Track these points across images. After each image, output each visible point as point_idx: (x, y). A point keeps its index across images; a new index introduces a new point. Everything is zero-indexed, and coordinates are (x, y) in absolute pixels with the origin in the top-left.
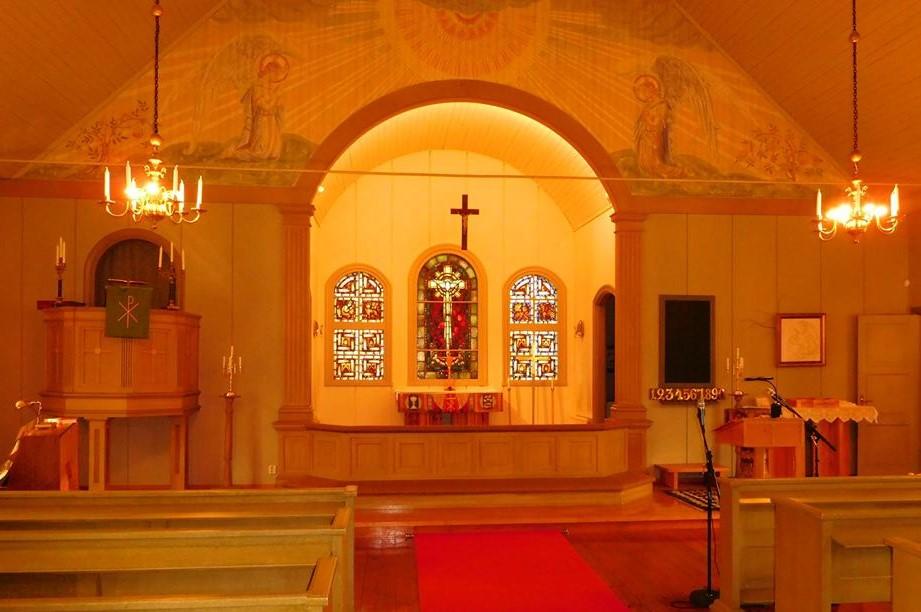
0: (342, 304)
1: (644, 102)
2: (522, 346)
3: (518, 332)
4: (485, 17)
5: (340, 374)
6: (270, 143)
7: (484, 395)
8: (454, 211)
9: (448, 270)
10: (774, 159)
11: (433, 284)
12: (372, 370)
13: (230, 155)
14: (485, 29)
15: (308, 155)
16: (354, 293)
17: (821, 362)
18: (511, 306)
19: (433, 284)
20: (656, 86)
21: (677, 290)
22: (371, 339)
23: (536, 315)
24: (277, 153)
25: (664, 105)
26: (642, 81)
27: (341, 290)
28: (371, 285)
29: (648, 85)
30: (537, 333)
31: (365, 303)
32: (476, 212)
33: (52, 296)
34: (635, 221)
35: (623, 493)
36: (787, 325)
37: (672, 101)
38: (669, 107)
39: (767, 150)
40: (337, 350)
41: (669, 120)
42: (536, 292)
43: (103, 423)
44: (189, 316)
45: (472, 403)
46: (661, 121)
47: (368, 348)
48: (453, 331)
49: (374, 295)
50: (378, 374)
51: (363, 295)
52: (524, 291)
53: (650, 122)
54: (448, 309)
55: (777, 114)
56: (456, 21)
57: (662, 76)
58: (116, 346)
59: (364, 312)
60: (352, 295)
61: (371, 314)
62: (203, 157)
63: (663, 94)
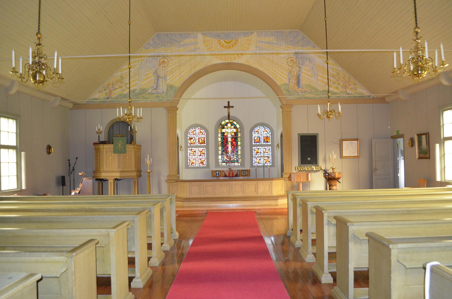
0: (191, 139)
1: (291, 66)
2: (258, 152)
3: (256, 147)
4: (234, 41)
5: (190, 164)
6: (163, 87)
7: (243, 170)
8: (225, 107)
9: (229, 125)
10: (339, 84)
11: (224, 131)
12: (202, 163)
13: (150, 92)
14: (234, 45)
15: (176, 90)
16: (195, 135)
17: (358, 156)
18: (253, 138)
19: (224, 131)
20: (295, 61)
21: (305, 131)
22: (202, 151)
23: (263, 141)
24: (165, 90)
25: (298, 68)
26: (290, 59)
27: (190, 134)
28: (201, 132)
29: (292, 60)
30: (263, 147)
31: (199, 138)
32: (233, 107)
33: (97, 141)
34: (288, 108)
35: (279, 201)
36: (345, 143)
37: (301, 66)
38: (300, 68)
39: (336, 81)
40: (189, 156)
41: (300, 72)
42: (262, 132)
43: (113, 180)
44: (138, 146)
45: (238, 174)
46: (297, 73)
47: (200, 154)
48: (232, 148)
49: (202, 135)
50: (204, 164)
51: (199, 135)
52: (258, 132)
53: (293, 73)
54: (230, 140)
55: (339, 68)
56: (224, 43)
57: (297, 57)
58: (116, 155)
59: (199, 142)
60: (194, 135)
61: (201, 142)
62: (141, 93)
63: (297, 63)
